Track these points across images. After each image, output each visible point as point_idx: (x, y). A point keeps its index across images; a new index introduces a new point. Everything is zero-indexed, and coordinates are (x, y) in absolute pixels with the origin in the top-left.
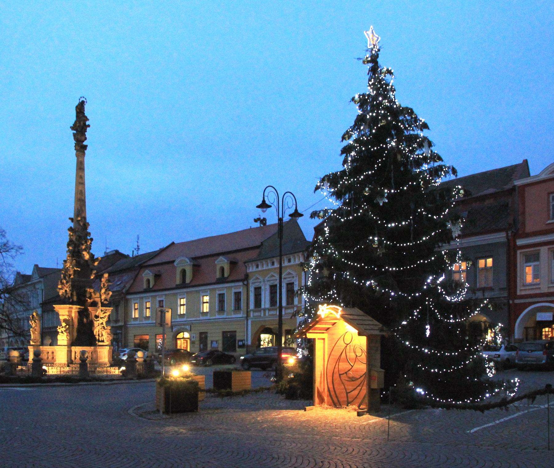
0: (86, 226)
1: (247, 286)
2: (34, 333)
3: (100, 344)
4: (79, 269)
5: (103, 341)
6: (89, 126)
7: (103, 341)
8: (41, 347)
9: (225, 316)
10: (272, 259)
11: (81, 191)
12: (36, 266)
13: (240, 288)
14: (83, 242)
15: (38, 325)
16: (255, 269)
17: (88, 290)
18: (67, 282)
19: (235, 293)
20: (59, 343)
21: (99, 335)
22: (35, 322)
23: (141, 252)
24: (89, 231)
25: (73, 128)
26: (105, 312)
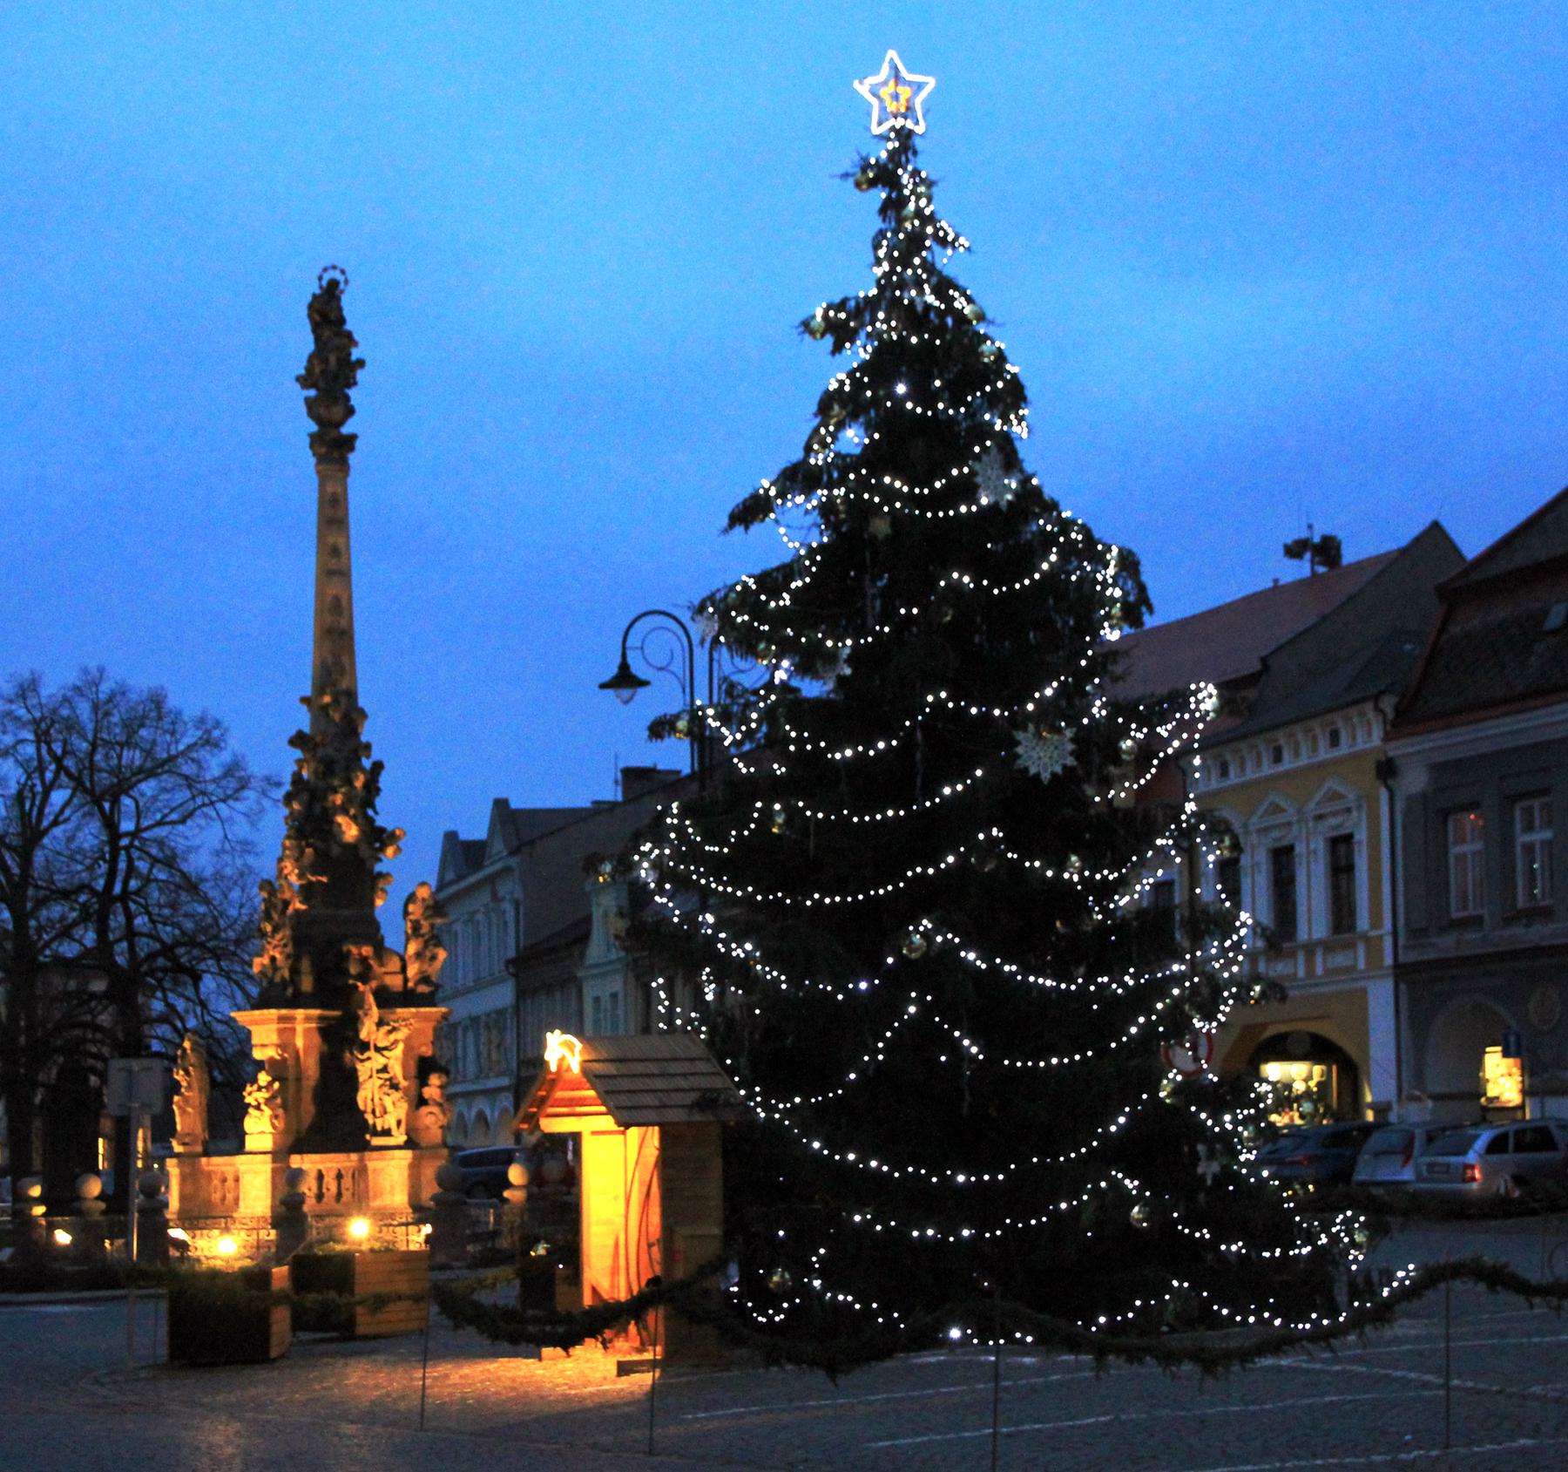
0: (352, 717)
2: (183, 1112)
3: (376, 1141)
4: (324, 879)
5: (387, 1133)
6: (361, 363)
7: (387, 1133)
8: (204, 1160)
10: (1328, 717)
11: (337, 599)
12: (501, 805)
14: (336, 782)
15: (195, 1085)
17: (354, 950)
18: (276, 929)
20: (250, 1143)
21: (373, 1112)
22: (187, 1073)
24: (364, 738)
25: (305, 381)
26: (394, 1029)
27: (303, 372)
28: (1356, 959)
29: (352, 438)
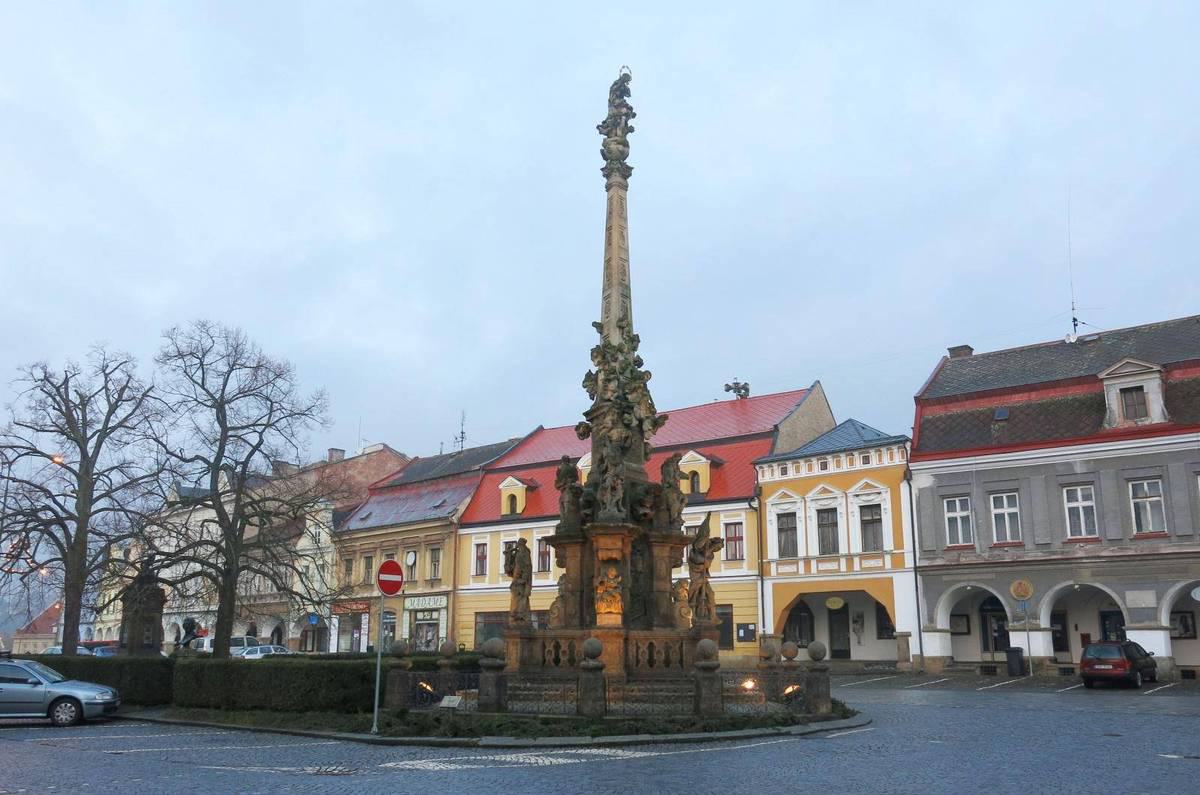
1: (760, 513)
13: (485, 538)
16: (778, 476)
23: (468, 445)
27: (601, 124)
28: (839, 565)
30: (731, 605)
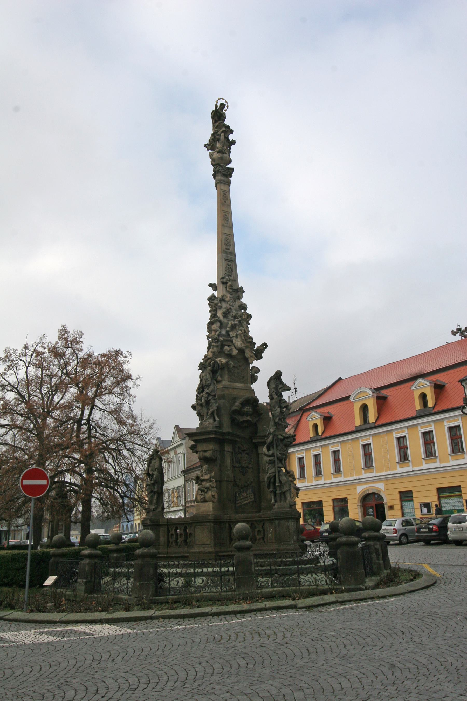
6: (233, 142)
9: (437, 464)
12: (177, 427)
19: (451, 429)
27: (208, 142)
29: (232, 169)
30: (411, 491)
